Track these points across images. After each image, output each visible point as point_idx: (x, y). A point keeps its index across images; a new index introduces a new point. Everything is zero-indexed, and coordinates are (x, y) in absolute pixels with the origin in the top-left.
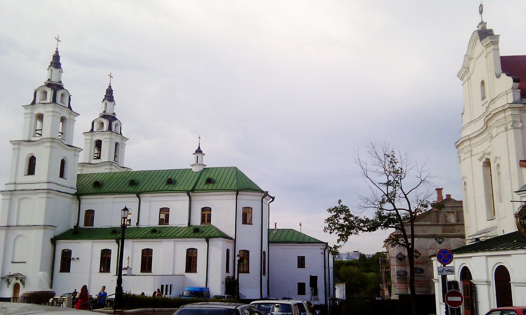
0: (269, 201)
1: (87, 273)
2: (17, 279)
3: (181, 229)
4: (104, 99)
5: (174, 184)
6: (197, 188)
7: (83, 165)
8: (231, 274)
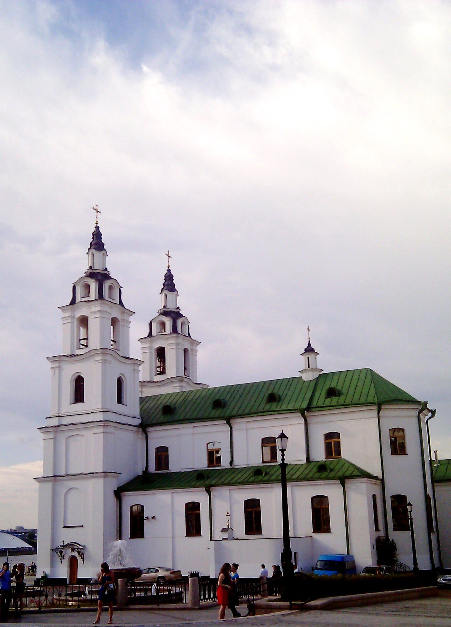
0: (427, 417)
2: (73, 550)
3: (297, 467)
4: (162, 290)
5: (279, 401)
6: (314, 404)
7: (143, 384)
8: (382, 533)
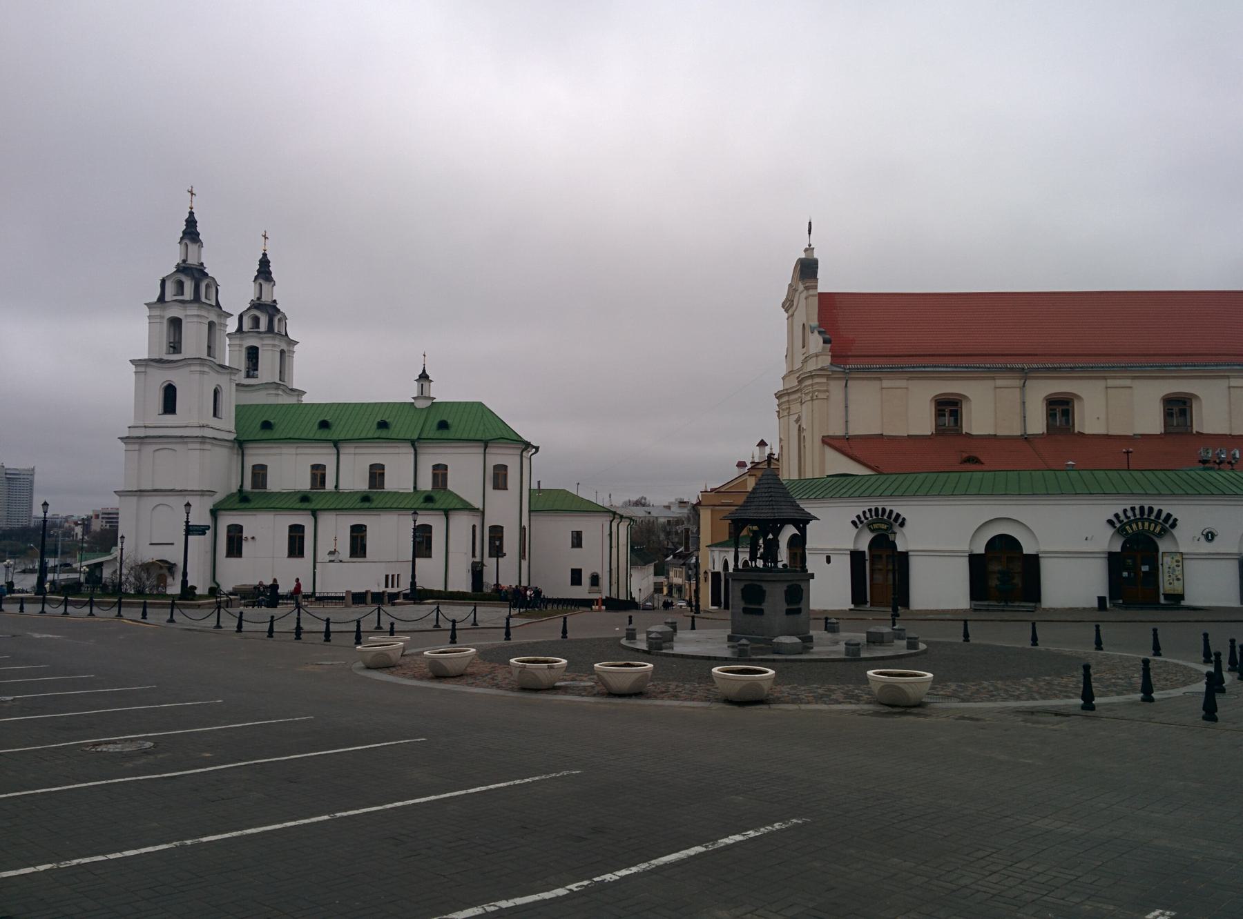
1: (265, 558)
8: (478, 559)
